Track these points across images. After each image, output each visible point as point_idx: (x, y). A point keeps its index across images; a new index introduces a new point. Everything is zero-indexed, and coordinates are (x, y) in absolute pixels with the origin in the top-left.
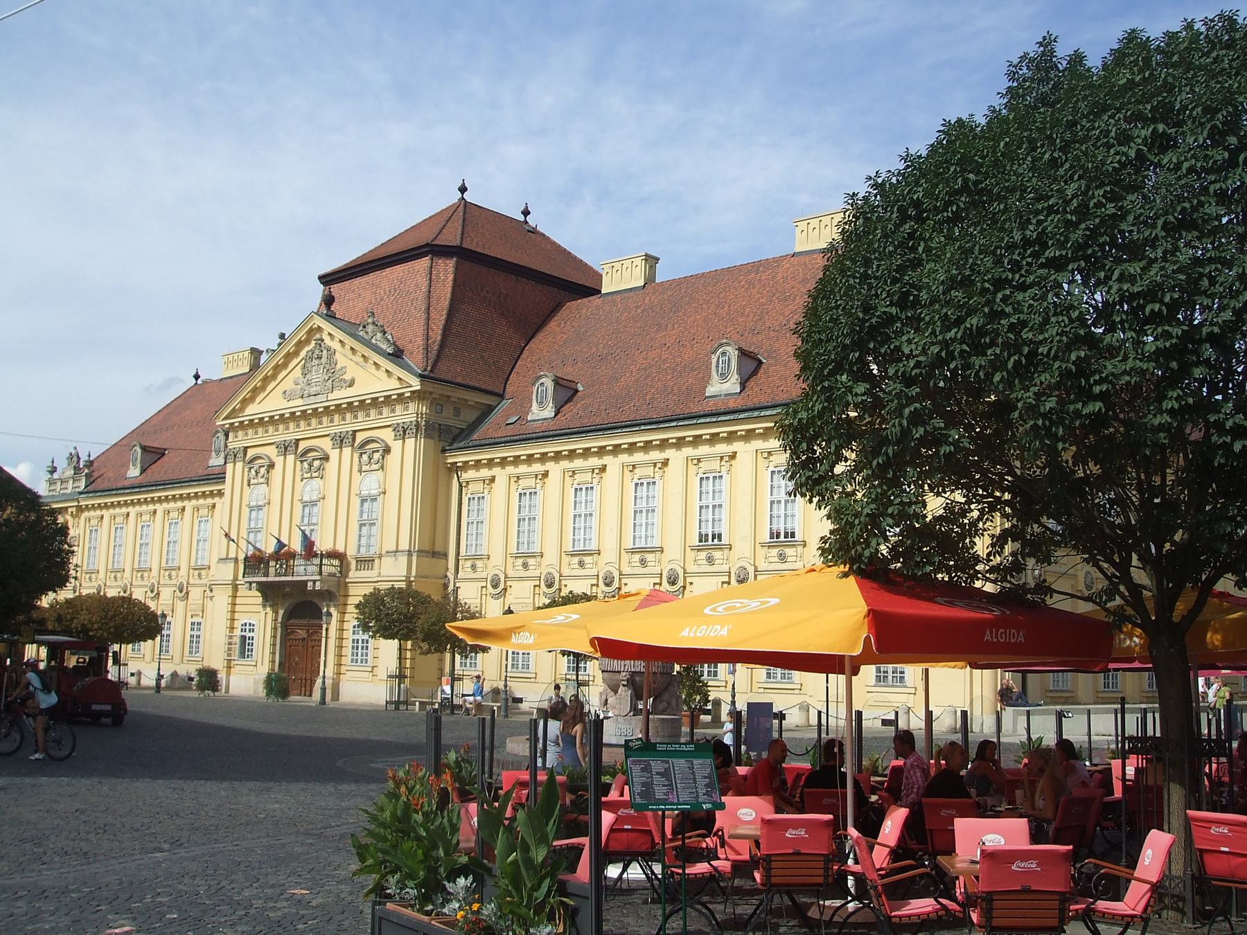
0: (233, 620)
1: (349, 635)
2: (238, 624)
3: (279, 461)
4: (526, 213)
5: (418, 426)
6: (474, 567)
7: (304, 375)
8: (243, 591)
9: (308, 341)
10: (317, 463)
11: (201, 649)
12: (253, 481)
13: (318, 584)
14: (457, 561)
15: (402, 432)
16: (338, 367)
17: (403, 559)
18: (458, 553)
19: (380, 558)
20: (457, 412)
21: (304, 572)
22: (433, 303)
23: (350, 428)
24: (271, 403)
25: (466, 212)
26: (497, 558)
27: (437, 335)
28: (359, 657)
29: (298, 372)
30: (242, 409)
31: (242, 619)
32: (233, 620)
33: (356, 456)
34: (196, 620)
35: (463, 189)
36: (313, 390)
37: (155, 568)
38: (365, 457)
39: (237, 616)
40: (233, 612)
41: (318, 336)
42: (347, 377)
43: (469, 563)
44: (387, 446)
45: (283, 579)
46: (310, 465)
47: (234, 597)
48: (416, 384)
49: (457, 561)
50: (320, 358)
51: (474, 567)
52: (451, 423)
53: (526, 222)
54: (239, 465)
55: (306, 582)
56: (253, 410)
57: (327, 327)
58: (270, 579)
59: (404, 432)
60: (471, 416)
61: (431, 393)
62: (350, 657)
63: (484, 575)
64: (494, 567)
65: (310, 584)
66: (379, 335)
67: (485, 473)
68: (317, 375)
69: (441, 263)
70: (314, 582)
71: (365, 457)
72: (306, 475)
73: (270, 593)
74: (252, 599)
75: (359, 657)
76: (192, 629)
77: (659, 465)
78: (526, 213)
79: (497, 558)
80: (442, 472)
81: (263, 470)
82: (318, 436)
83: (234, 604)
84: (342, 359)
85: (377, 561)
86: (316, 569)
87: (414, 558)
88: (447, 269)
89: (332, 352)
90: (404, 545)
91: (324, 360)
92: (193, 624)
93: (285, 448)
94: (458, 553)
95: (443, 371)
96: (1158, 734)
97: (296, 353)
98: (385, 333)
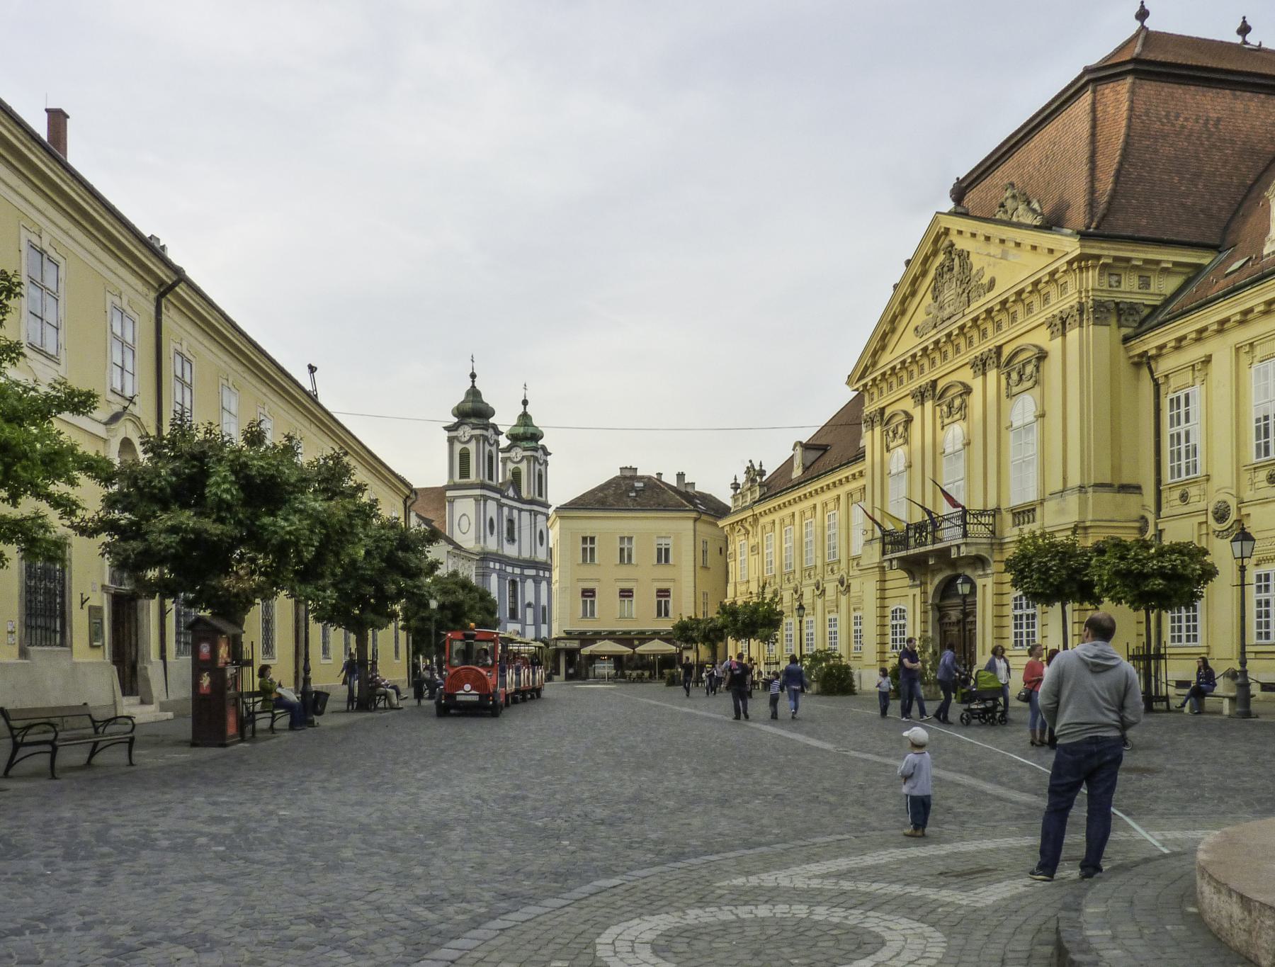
0: (883, 607)
1: (1009, 611)
2: (888, 612)
3: (916, 413)
4: (1244, 29)
5: (1081, 311)
6: (1184, 498)
7: (935, 298)
8: (890, 575)
9: (935, 253)
10: (957, 402)
11: (1201, 632)
12: (892, 445)
13: (963, 548)
14: (1159, 493)
15: (1060, 325)
16: (974, 272)
17: (1073, 500)
18: (1158, 482)
19: (1042, 503)
20: (1145, 284)
21: (950, 536)
22: (1100, 145)
23: (991, 344)
24: (906, 344)
25: (1149, 38)
26: (1223, 476)
27: (1106, 184)
28: (1184, 634)
29: (929, 299)
30: (874, 364)
31: (893, 605)
32: (883, 607)
33: (1003, 377)
34: (832, 616)
35: (1142, 14)
36: (946, 313)
37: (819, 564)
38: (1014, 376)
39: (887, 602)
40: (883, 598)
41: (947, 243)
42: (985, 281)
43: (1176, 494)
44: (1041, 350)
45: (922, 549)
46: (950, 407)
47: (883, 581)
48: (1070, 246)
49: (1159, 493)
50: (951, 269)
51: (1184, 498)
52: (1136, 299)
53: (1245, 42)
54: (878, 430)
55: (948, 549)
56: (888, 359)
57: (957, 223)
58: (911, 552)
59: (1064, 323)
60: (1169, 285)
61: (1098, 257)
62: (1012, 639)
63: (1202, 505)
64: (1222, 485)
65: (954, 551)
66: (1022, 207)
67: (1194, 353)
68: (950, 293)
69: (1107, 90)
70: (958, 546)
71: (1014, 376)
72: (946, 421)
73: (915, 567)
74: (898, 578)
75: (1184, 634)
76: (856, 624)
77: (1198, 367)
78: (1244, 29)
79: (1223, 476)
80: (1124, 365)
81: (901, 429)
82: (954, 369)
83: (883, 590)
84: (976, 262)
85: (1038, 511)
86: (959, 531)
87: (1090, 495)
88: (1118, 96)
89: (964, 256)
90: (1075, 480)
91: (956, 268)
92: (856, 618)
93: (981, 365)
94: (1158, 482)
95: (1120, 224)
96: (370, 632)
97: (924, 273)
98: (1029, 203)
